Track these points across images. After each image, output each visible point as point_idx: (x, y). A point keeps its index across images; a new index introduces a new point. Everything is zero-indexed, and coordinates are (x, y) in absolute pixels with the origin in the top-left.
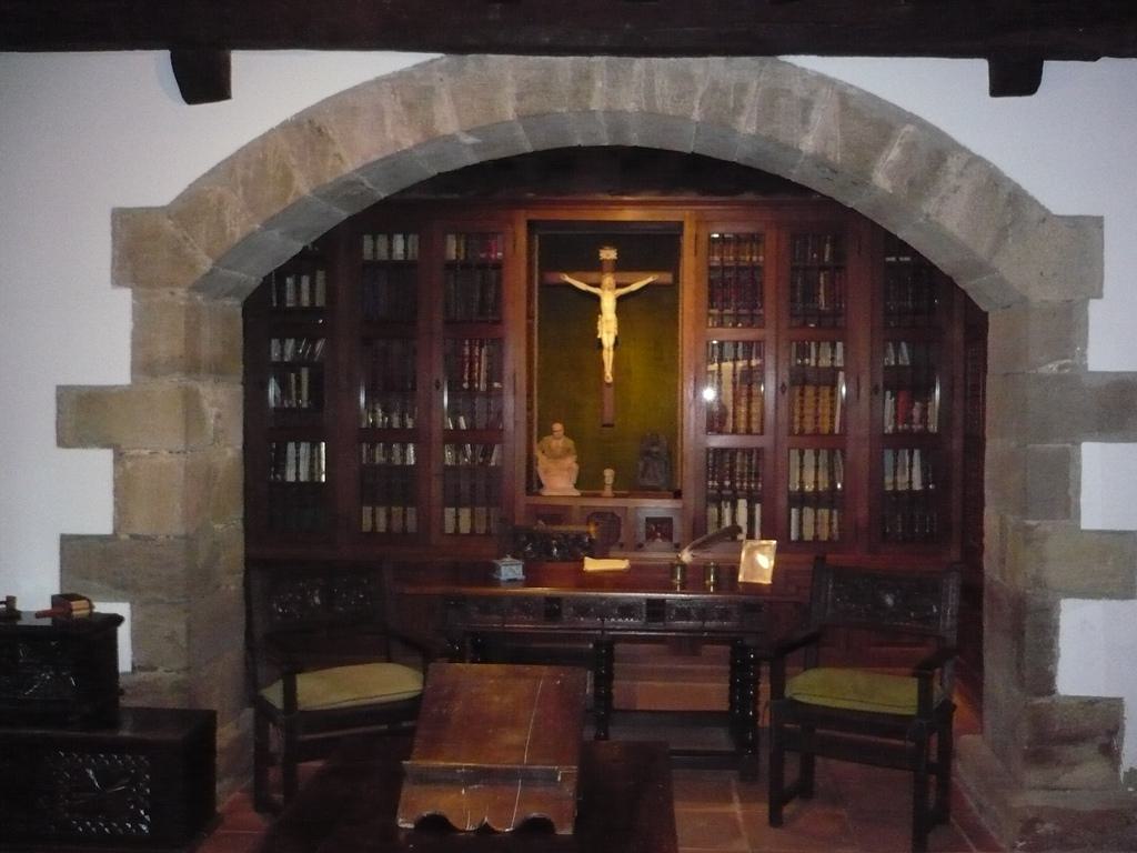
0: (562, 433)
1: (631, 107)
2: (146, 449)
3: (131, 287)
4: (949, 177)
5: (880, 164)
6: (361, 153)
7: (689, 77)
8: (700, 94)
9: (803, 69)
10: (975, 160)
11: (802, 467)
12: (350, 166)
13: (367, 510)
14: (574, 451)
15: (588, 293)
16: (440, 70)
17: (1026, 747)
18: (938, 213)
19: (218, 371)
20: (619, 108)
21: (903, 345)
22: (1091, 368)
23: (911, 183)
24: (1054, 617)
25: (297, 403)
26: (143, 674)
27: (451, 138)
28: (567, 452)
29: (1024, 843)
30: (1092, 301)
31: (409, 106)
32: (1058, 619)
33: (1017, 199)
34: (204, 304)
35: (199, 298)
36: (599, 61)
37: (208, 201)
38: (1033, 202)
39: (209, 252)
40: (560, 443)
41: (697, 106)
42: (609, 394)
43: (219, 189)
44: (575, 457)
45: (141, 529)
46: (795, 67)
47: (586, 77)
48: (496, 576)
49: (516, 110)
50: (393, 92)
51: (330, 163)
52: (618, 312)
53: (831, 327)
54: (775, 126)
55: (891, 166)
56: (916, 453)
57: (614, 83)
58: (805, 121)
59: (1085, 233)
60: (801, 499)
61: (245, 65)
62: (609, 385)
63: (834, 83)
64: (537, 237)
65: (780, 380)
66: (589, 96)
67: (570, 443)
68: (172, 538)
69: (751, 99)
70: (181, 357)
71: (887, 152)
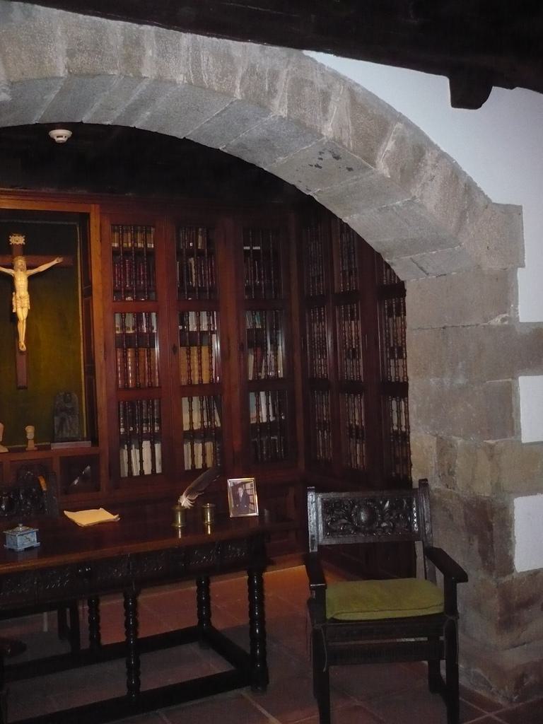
4: (428, 168)
7: (229, 57)
8: (240, 74)
10: (443, 156)
11: (191, 411)
17: (499, 618)
18: (421, 197)
21: (154, 315)
22: (522, 320)
23: (402, 171)
24: (510, 513)
36: (149, 31)
38: (481, 192)
41: (238, 86)
42: (22, 361)
46: (315, 61)
48: (7, 546)
49: (68, 67)
52: (30, 289)
53: (207, 300)
55: (388, 155)
56: (262, 394)
57: (162, 54)
58: (325, 110)
60: (192, 435)
62: (22, 353)
63: (345, 81)
66: (140, 62)
69: (283, 85)
71: (385, 143)
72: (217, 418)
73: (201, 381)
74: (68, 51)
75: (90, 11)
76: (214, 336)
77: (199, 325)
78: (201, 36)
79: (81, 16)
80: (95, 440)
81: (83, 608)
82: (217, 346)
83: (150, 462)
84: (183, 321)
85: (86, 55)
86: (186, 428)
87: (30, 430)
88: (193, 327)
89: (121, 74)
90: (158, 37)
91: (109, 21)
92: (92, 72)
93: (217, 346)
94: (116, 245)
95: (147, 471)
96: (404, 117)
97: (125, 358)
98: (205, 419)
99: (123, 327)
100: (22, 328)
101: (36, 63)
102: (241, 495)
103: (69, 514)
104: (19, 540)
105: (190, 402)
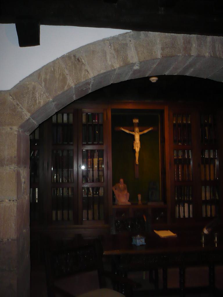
15: (129, 134)
16: (130, 37)
21: (190, 151)
31: (117, 51)
36: (194, 36)
37: (29, 88)
39: (29, 111)
49: (162, 54)
50: (110, 45)
51: (83, 73)
52: (141, 140)
60: (206, 202)
61: (45, 30)
62: (137, 165)
66: (190, 50)
68: (10, 240)
72: (217, 195)
73: (210, 179)
74: (161, 48)
75: (171, 32)
76: (216, 160)
77: (209, 155)
78: (216, 37)
79: (166, 34)
80: (165, 200)
81: (161, 271)
82: (217, 163)
83: (188, 213)
84: (203, 153)
85: (168, 49)
86: (203, 199)
87: (139, 196)
88: (207, 156)
89: (183, 55)
90: (197, 38)
91: (178, 35)
92: (171, 55)
93: (217, 163)
94: (175, 122)
95: (187, 216)
97: (178, 168)
98: (212, 196)
99: (178, 156)
101: (150, 53)
103: (155, 231)
104: (138, 241)
105: (205, 188)
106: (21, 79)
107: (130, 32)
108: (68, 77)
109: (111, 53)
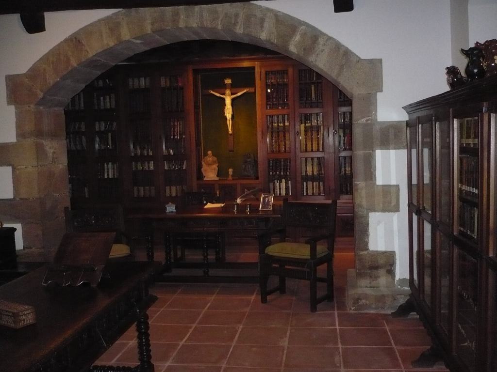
0: (211, 155)
1: (195, 25)
2: (23, 166)
3: (15, 105)
5: (292, 42)
6: (94, 48)
7: (216, 12)
8: (221, 18)
9: (260, 6)
10: (330, 38)
11: (306, 165)
12: (91, 55)
13: (135, 188)
14: (217, 162)
19: (53, 136)
20: (190, 26)
23: (304, 49)
25: (76, 148)
26: (28, 250)
27: (128, 41)
28: (214, 162)
29: (354, 308)
30: (378, 93)
31: (111, 30)
32: (368, 221)
33: (347, 53)
34: (44, 110)
35: (41, 108)
36: (182, 8)
39: (41, 91)
40: (211, 159)
42: (231, 138)
43: (44, 66)
44: (217, 165)
45: (24, 196)
47: (177, 14)
49: (151, 29)
52: (232, 105)
54: (250, 30)
57: (188, 17)
58: (262, 27)
59: (375, 65)
61: (51, 18)
64: (200, 76)
65: (296, 129)
66: (178, 22)
67: (215, 159)
69: (240, 20)
70: (34, 131)
71: (294, 37)
87: (231, 171)
96: (306, 23)
100: (229, 123)
102: (266, 201)
106: (33, 63)
107: (122, 10)
108: (71, 58)
109: (106, 32)
